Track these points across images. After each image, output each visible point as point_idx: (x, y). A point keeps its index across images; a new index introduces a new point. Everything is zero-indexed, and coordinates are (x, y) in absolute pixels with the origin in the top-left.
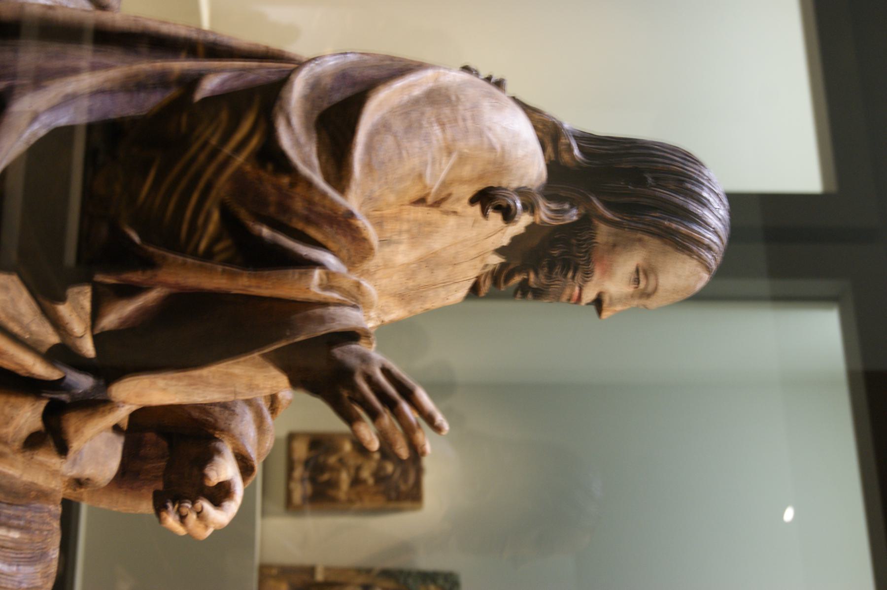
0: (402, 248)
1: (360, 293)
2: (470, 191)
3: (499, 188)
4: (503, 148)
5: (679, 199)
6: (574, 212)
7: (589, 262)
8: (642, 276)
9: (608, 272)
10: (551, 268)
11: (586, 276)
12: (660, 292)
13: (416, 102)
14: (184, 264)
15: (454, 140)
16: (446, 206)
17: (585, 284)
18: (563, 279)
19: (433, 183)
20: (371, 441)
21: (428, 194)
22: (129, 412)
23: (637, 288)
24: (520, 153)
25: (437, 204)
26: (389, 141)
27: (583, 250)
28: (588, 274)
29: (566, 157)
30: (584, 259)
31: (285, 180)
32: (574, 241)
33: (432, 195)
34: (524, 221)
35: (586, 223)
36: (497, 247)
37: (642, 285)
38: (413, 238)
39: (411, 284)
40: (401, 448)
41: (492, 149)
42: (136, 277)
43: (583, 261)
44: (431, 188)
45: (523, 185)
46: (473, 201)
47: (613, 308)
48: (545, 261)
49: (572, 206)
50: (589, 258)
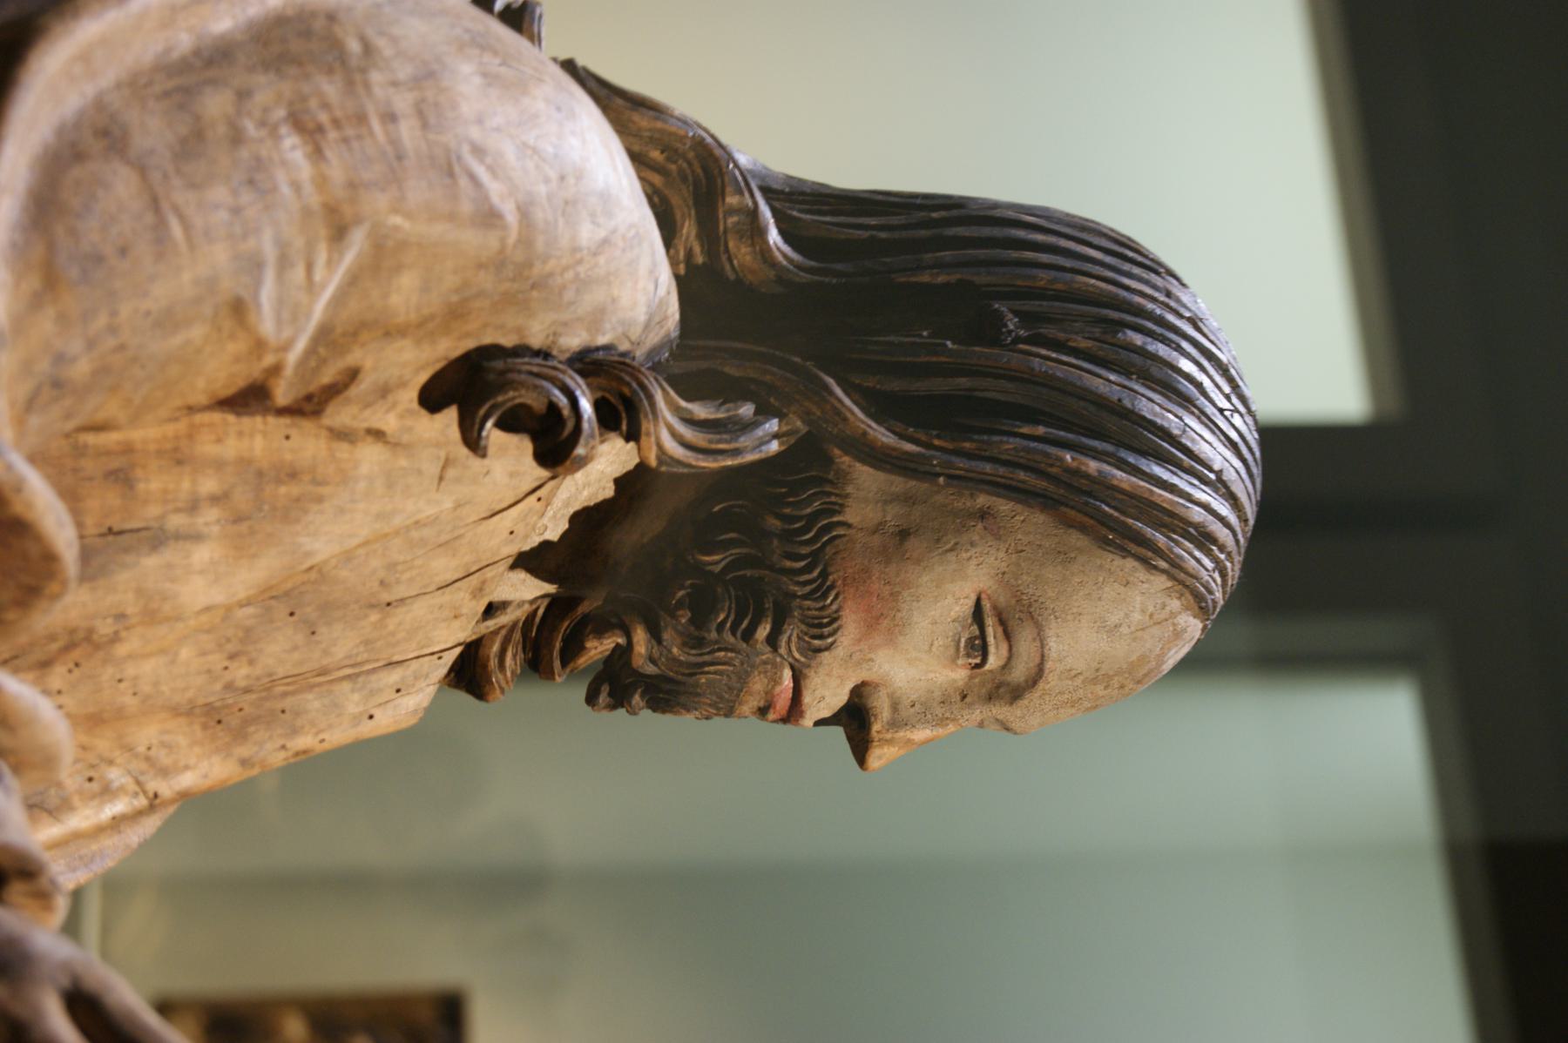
0: (202, 554)
3: (521, 351)
4: (524, 212)
5: (1107, 384)
6: (773, 425)
7: (822, 590)
11: (816, 631)
12: (1051, 681)
16: (340, 414)
21: (276, 370)
23: (977, 666)
26: (122, 185)
28: (821, 631)
29: (742, 254)
33: (289, 371)
37: (993, 662)
41: (489, 217)
44: (285, 347)
45: (602, 340)
49: (764, 412)
50: (824, 575)
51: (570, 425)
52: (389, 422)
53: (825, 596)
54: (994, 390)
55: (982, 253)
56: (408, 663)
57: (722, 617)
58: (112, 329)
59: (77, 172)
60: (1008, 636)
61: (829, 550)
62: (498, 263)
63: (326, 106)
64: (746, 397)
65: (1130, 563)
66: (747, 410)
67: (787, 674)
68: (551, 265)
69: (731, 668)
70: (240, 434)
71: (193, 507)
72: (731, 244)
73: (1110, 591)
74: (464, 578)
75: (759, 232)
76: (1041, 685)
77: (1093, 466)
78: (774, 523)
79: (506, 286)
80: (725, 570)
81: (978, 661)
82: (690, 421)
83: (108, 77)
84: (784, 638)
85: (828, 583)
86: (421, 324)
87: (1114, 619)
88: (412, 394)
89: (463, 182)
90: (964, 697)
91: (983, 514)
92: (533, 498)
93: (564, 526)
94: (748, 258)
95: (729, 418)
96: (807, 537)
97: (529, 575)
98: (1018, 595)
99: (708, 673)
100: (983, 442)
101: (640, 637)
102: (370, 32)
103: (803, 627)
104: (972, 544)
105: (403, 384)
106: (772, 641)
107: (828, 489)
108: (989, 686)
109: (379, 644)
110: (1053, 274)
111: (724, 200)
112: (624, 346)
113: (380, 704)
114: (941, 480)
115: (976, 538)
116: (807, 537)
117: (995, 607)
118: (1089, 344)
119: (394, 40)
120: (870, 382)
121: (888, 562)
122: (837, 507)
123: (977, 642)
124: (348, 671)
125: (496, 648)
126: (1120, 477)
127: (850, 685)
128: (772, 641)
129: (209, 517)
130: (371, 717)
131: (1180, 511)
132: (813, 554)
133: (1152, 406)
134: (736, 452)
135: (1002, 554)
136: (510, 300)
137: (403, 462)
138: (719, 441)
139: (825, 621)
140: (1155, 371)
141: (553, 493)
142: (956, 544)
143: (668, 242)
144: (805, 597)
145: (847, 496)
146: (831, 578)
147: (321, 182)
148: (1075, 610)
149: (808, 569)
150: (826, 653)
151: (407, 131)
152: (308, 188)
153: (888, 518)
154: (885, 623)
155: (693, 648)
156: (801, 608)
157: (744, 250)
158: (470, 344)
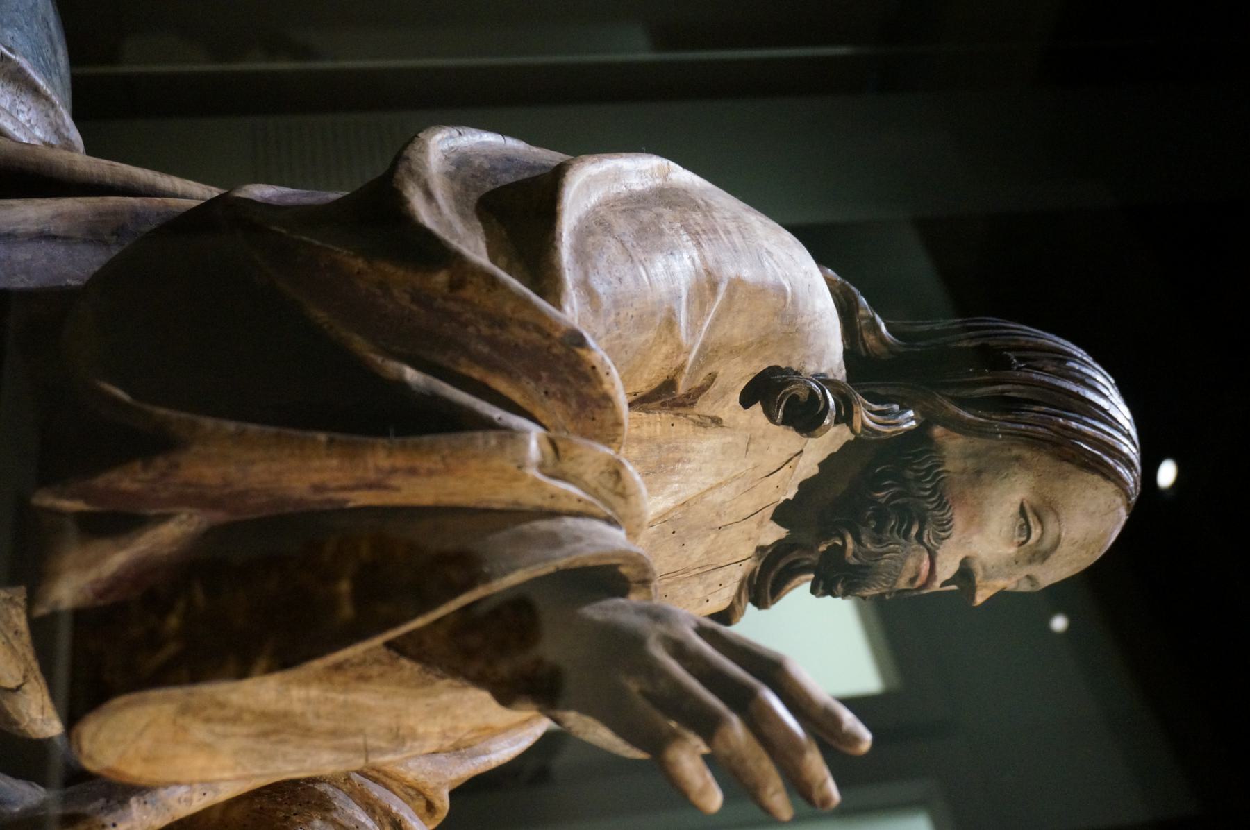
1: (619, 489)
2: (738, 374)
3: (788, 371)
4: (794, 294)
6: (911, 413)
7: (941, 505)
8: (1032, 519)
9: (976, 520)
10: (881, 517)
11: (941, 528)
14: (239, 437)
16: (704, 407)
17: (941, 544)
18: (903, 541)
20: (704, 791)
21: (680, 369)
23: (1024, 543)
26: (613, 247)
27: (929, 486)
28: (944, 526)
29: (871, 340)
30: (933, 499)
31: (441, 278)
32: (909, 474)
33: (686, 370)
34: (833, 437)
36: (770, 516)
37: (1036, 532)
40: (774, 794)
43: (932, 503)
44: (688, 352)
45: (823, 370)
46: (747, 399)
47: (991, 583)
48: (870, 510)
49: (904, 409)
50: (941, 497)
51: (822, 407)
53: (943, 508)
55: (991, 332)
56: (725, 568)
57: (893, 523)
58: (617, 323)
59: (591, 240)
61: (941, 484)
65: (1097, 477)
66: (896, 407)
67: (926, 555)
68: (805, 319)
69: (897, 555)
70: (649, 423)
72: (865, 335)
73: (1090, 493)
74: (755, 513)
75: (876, 328)
76: (1059, 550)
77: (1074, 424)
80: (887, 502)
81: (1024, 539)
84: (926, 532)
85: (944, 501)
87: (1092, 508)
88: (736, 396)
90: (1017, 562)
92: (787, 467)
94: (874, 341)
95: (889, 410)
96: (928, 479)
97: (775, 524)
99: (885, 559)
100: (1017, 415)
101: (849, 539)
103: (934, 526)
104: (1016, 474)
105: (733, 389)
106: (919, 537)
107: (934, 455)
108: (1028, 555)
109: (714, 554)
110: (1026, 338)
111: (858, 312)
113: (712, 593)
114: (1000, 436)
115: (1016, 470)
116: (928, 479)
117: (1032, 507)
118: (1054, 368)
121: (973, 486)
122: (940, 463)
123: (1024, 527)
124: (698, 571)
127: (959, 558)
130: (708, 601)
131: (1118, 446)
132: (932, 487)
134: (897, 424)
135: (1031, 477)
138: (889, 419)
139: (945, 522)
140: (1087, 380)
141: (798, 461)
142: (1007, 474)
144: (933, 510)
145: (944, 457)
146: (945, 498)
148: (1073, 504)
150: (947, 540)
152: (698, 261)
153: (968, 466)
154: (977, 520)
155: (878, 544)
156: (933, 516)
157: (872, 337)
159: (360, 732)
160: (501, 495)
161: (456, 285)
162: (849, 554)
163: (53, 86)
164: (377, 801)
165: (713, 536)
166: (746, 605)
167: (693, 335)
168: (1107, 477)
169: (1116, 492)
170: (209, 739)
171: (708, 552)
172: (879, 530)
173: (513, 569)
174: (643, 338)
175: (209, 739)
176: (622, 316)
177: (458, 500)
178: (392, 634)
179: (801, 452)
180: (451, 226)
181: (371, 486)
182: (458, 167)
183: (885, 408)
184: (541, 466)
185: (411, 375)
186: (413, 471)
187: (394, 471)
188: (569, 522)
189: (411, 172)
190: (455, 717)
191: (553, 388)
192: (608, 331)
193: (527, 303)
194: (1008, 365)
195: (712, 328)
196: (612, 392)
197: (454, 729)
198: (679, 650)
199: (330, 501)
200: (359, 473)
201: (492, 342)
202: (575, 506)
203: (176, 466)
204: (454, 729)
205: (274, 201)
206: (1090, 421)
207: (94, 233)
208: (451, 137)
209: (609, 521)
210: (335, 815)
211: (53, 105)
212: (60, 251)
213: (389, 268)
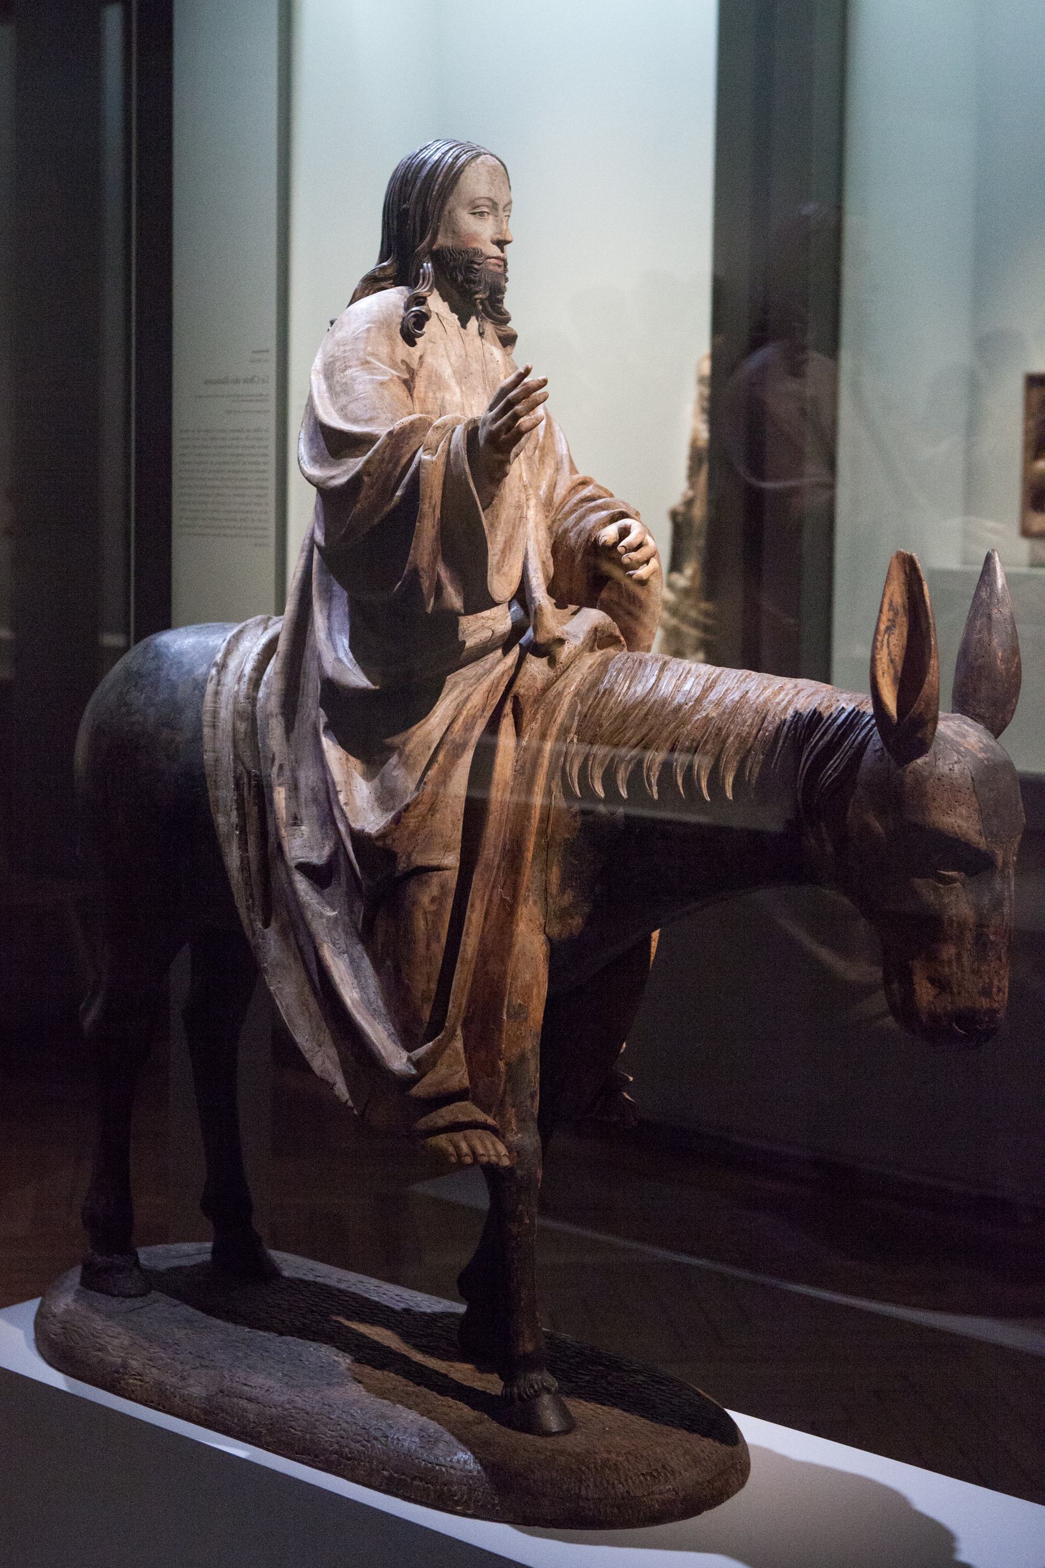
0: (448, 397)
3: (402, 324)
4: (370, 322)
6: (425, 264)
7: (467, 252)
9: (474, 237)
12: (491, 195)
13: (330, 388)
15: (358, 359)
16: (415, 365)
19: (388, 373)
21: (399, 377)
22: (546, 595)
24: (376, 308)
25: (412, 373)
26: (352, 407)
28: (477, 252)
29: (389, 271)
31: (366, 479)
33: (399, 375)
35: (438, 257)
37: (485, 209)
38: (440, 389)
39: (480, 390)
41: (368, 330)
42: (426, 583)
44: (393, 375)
45: (403, 305)
49: (422, 267)
50: (463, 252)
51: (418, 313)
52: (418, 354)
54: (419, 212)
58: (382, 409)
59: (349, 415)
60: (478, 207)
62: (379, 328)
63: (341, 365)
64: (419, 271)
66: (421, 271)
67: (488, 260)
68: (381, 317)
71: (436, 399)
73: (468, 181)
78: (452, 263)
79: (385, 327)
80: (462, 275)
81: (486, 214)
82: (423, 284)
83: (332, 410)
86: (392, 346)
89: (359, 336)
91: (450, 212)
93: (454, 314)
98: (468, 205)
101: (477, 296)
102: (329, 356)
106: (479, 264)
112: (406, 300)
119: (330, 351)
120: (418, 240)
125: (500, 332)
126: (440, 179)
127: (491, 245)
128: (479, 264)
129: (438, 395)
133: (424, 172)
134: (429, 274)
136: (389, 326)
137: (429, 351)
141: (443, 317)
143: (387, 289)
147: (357, 366)
149: (462, 255)
151: (348, 348)
152: (357, 369)
158: (399, 336)
159: (515, 519)
160: (441, 468)
161: (369, 475)
162: (484, 296)
163: (232, 628)
164: (570, 508)
165: (469, 359)
166: (508, 327)
167: (386, 372)
168: (462, 172)
169: (470, 166)
170: (508, 566)
171: (476, 361)
172: (474, 282)
173: (464, 469)
174: (387, 396)
175: (508, 566)
176: (378, 406)
177: (441, 482)
178: (480, 509)
179: (437, 314)
180: (345, 471)
181: (434, 511)
182: (317, 462)
183: (421, 277)
184: (433, 455)
185: (399, 493)
186: (431, 497)
187: (430, 503)
188: (452, 447)
189: (323, 483)
190: (514, 487)
191: (406, 442)
192: (385, 413)
193: (376, 451)
194: (406, 211)
195: (383, 363)
196: (409, 421)
197: (518, 488)
198: (495, 420)
199: (438, 524)
200: (429, 514)
201: (389, 463)
202: (447, 443)
203: (423, 569)
204: (518, 488)
205: (323, 531)
206: (437, 174)
207: (328, 597)
208: (304, 462)
209: (453, 431)
210: (570, 527)
211: (247, 625)
212: (334, 613)
213: (361, 496)
